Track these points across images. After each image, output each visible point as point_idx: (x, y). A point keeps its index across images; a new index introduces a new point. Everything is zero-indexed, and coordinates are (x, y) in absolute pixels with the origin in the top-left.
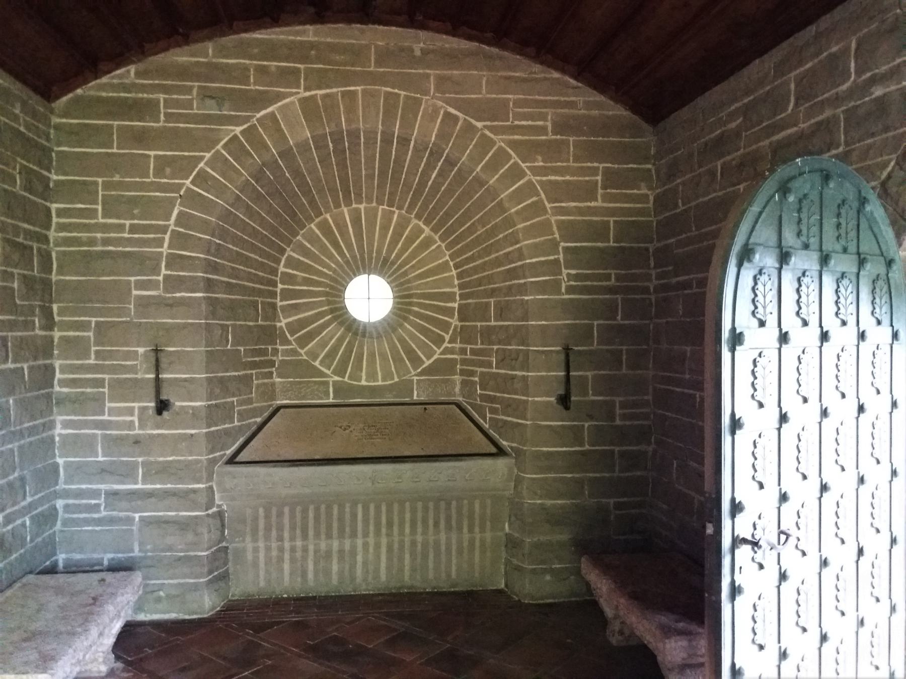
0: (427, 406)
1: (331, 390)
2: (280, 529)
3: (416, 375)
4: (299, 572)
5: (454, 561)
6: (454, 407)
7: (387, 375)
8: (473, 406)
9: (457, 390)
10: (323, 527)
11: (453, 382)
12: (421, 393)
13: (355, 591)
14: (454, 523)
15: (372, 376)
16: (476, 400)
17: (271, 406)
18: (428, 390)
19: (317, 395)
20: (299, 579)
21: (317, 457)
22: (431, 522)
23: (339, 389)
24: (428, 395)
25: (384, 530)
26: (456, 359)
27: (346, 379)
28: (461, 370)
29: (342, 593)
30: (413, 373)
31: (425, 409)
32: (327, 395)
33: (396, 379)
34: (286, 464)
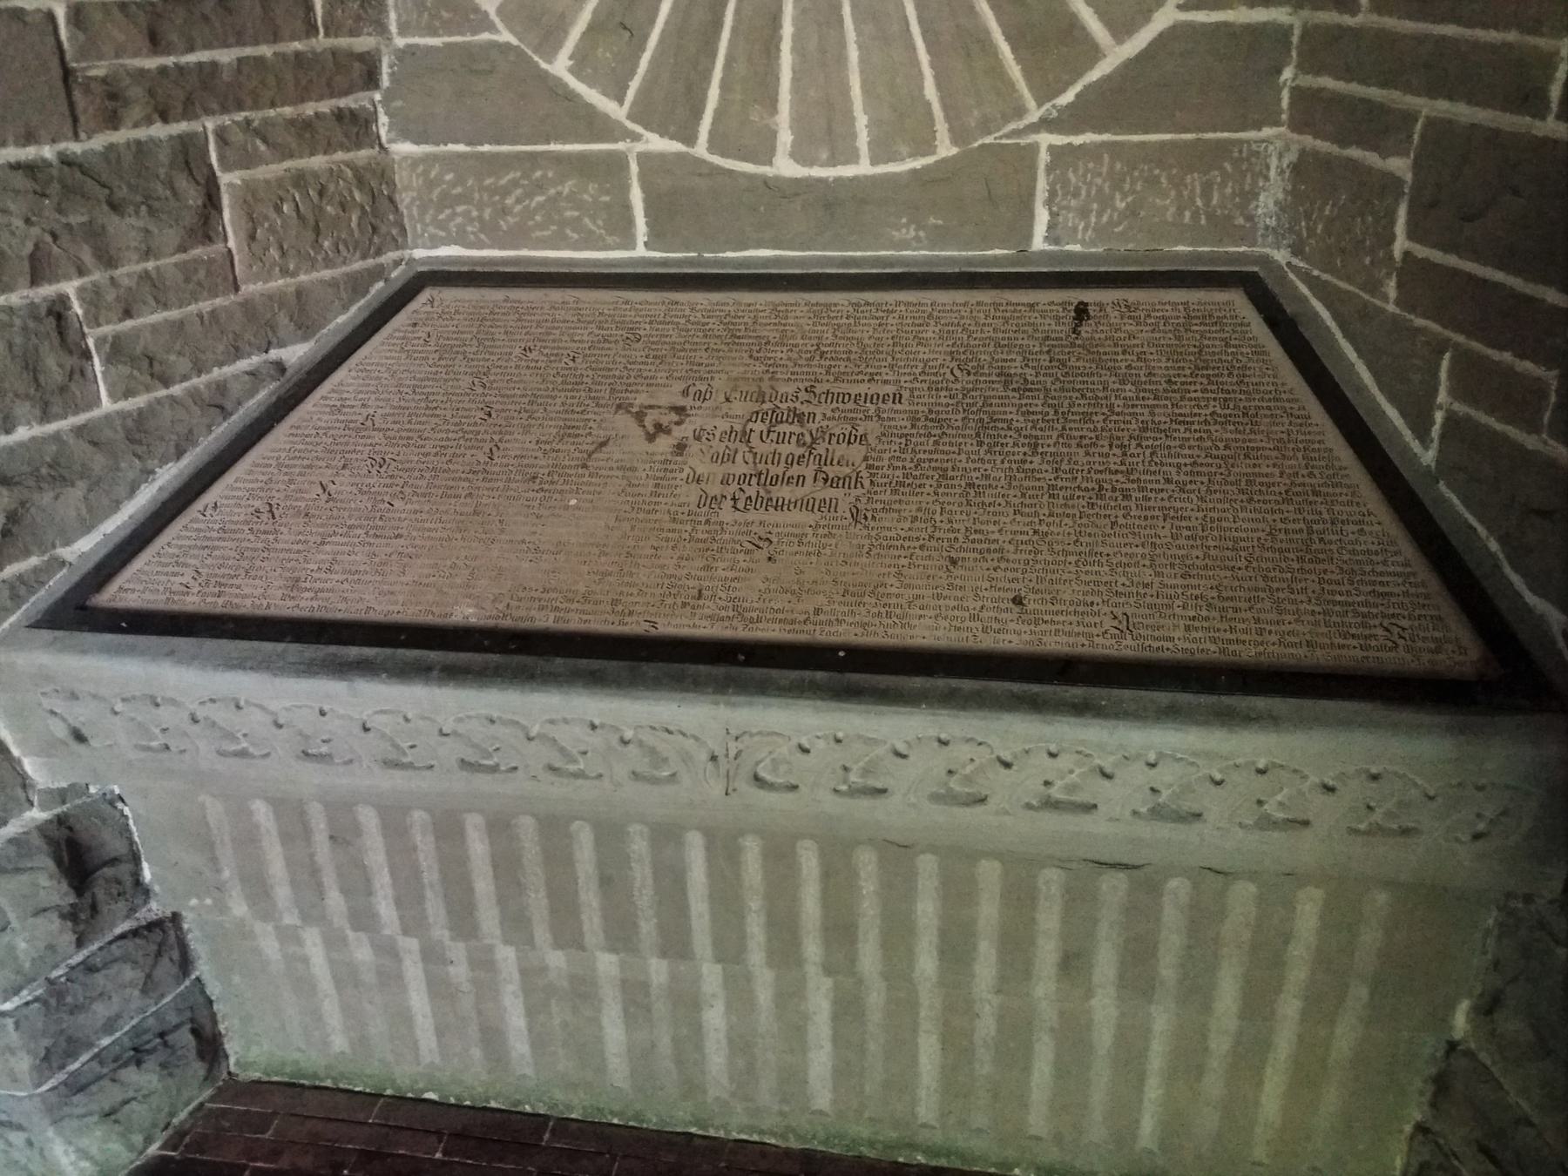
0: (1090, 296)
1: (636, 196)
2: (358, 886)
3: (1046, 124)
4: (473, 1030)
5: (1153, 1090)
6: (1237, 301)
7: (902, 125)
8: (1355, 319)
9: (1268, 202)
10: (537, 902)
11: (1249, 163)
12: (1071, 218)
13: (697, 1122)
14: (1167, 969)
15: (824, 131)
16: (1374, 287)
17: (378, 273)
18: (1106, 202)
19: (576, 224)
20: (477, 1053)
21: (465, 613)
22: (1047, 952)
23: (674, 198)
24: (1102, 232)
25: (812, 949)
26: (1284, 32)
27: (701, 149)
28: (1298, 94)
29: (652, 1122)
30: (1034, 115)
31: (1082, 312)
32: (622, 230)
33: (946, 149)
34: (293, 650)
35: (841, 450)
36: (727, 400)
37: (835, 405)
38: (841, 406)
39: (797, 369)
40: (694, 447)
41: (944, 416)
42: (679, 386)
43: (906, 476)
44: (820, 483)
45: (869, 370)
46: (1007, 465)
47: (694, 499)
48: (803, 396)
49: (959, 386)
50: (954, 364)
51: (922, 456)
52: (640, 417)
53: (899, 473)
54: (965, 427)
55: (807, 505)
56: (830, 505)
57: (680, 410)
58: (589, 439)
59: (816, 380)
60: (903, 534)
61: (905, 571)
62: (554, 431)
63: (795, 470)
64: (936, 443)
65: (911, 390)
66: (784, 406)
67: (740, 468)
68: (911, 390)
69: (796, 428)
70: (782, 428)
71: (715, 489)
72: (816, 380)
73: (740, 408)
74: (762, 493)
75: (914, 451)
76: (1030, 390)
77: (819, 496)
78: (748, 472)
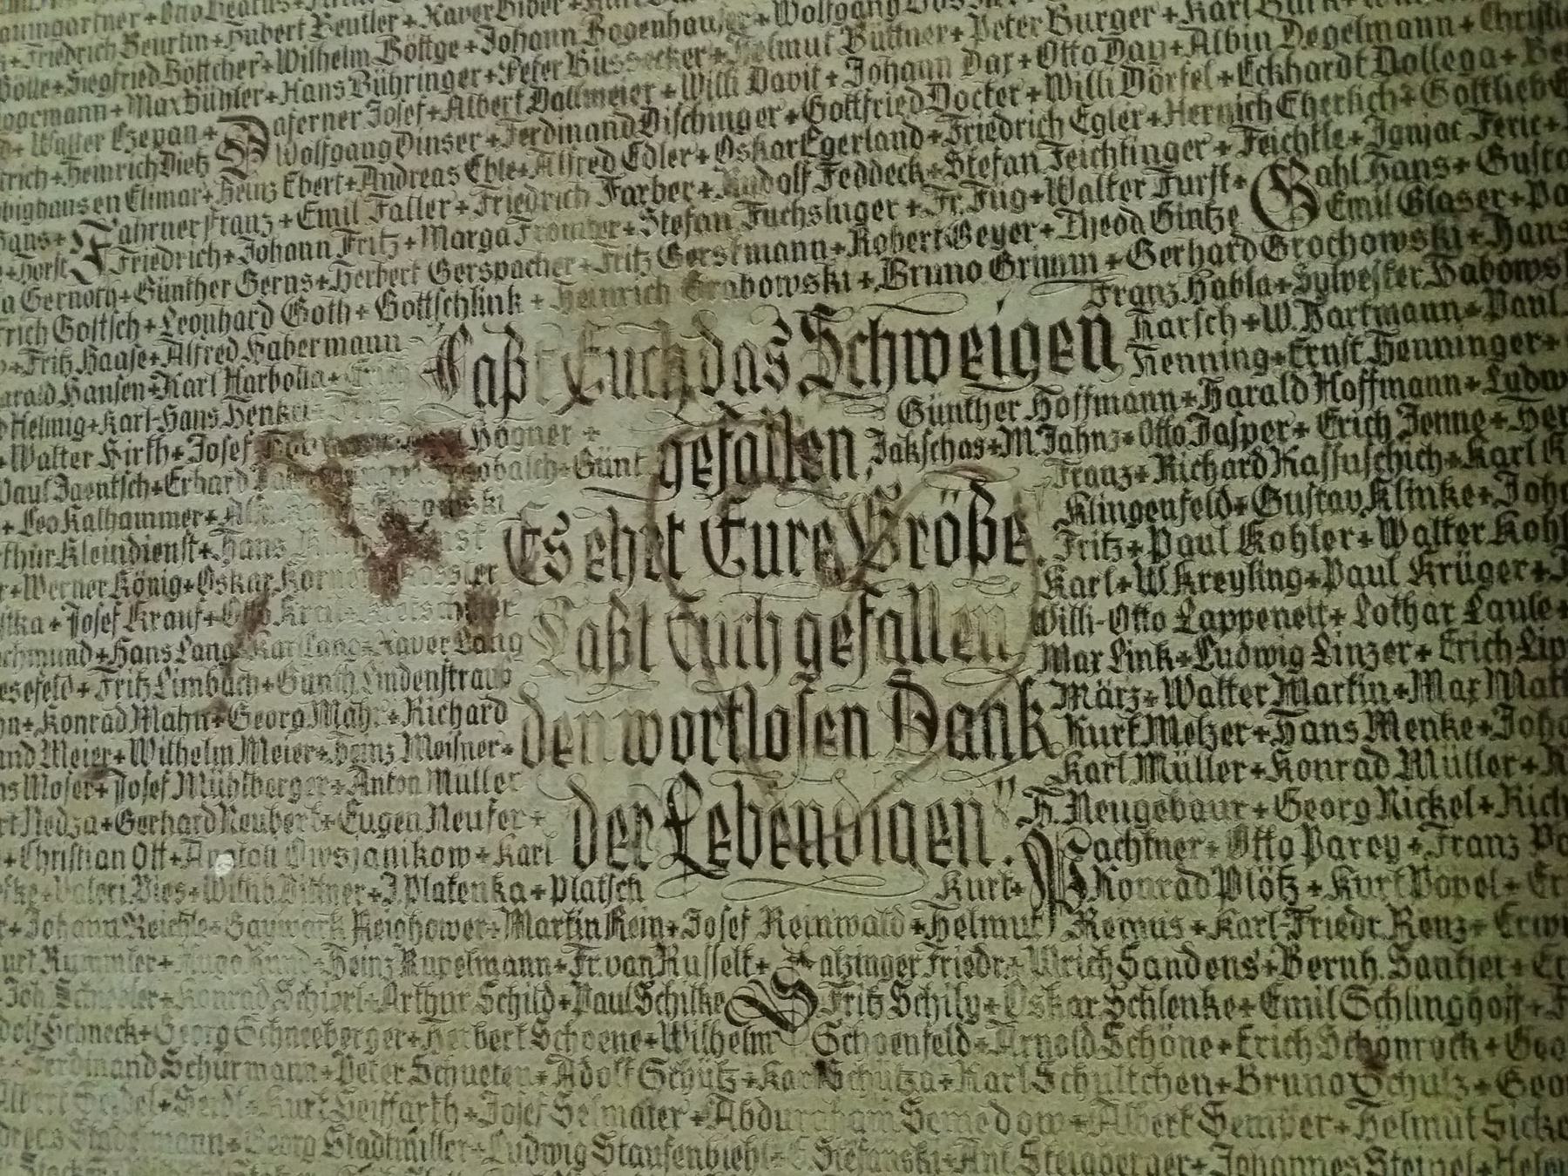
35: (954, 592)
36: (578, 396)
37: (903, 391)
38: (923, 390)
39: (763, 235)
40: (521, 607)
41: (1257, 415)
42: (420, 344)
43: (1176, 692)
44: (915, 739)
45: (991, 217)
46: (1486, 630)
47: (556, 830)
48: (803, 357)
49: (1284, 269)
50: (1255, 166)
51: (1211, 601)
52: (333, 485)
53: (1149, 680)
54: (1335, 462)
55: (893, 833)
56: (948, 835)
57: (441, 449)
58: (214, 603)
59: (831, 283)
60: (1205, 949)
61: (1234, 1106)
62: (108, 571)
63: (835, 688)
64: (1250, 536)
65: (1140, 301)
66: (749, 406)
67: (673, 694)
68: (1140, 301)
69: (799, 506)
70: (763, 504)
71: (612, 787)
72: (831, 283)
73: (625, 426)
74: (752, 793)
75: (1184, 581)
76: (1519, 271)
77: (924, 791)
78: (696, 704)
